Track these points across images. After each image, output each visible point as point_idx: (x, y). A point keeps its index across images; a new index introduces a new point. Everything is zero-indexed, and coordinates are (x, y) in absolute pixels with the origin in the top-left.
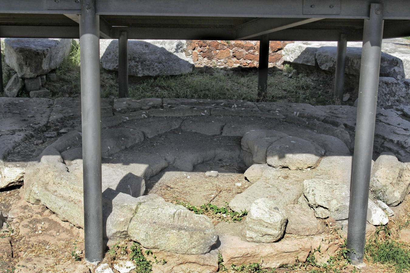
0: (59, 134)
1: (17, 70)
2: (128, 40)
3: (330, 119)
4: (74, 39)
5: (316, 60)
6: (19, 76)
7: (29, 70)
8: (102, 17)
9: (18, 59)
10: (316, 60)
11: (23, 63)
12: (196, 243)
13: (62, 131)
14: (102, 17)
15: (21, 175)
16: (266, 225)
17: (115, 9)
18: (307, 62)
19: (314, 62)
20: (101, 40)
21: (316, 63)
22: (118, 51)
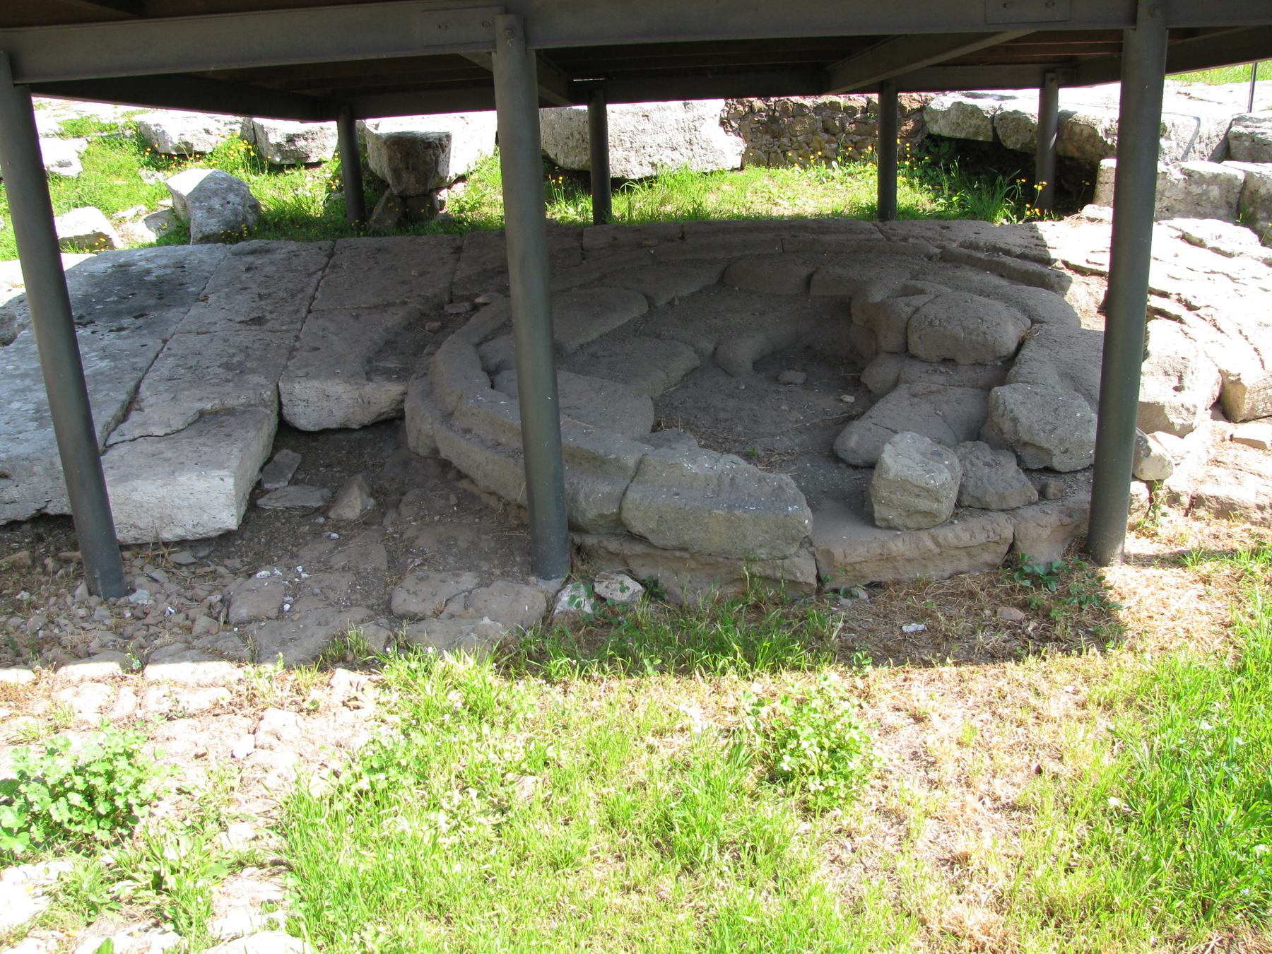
0: (476, 308)
1: (390, 182)
2: (370, 123)
3: (1033, 252)
4: (258, 121)
5: (994, 129)
6: (395, 192)
7: (413, 180)
8: (538, 52)
9: (390, 159)
10: (994, 129)
11: (401, 166)
12: (767, 536)
13: (480, 300)
14: (538, 52)
15: (399, 398)
16: (916, 490)
17: (574, 28)
18: (977, 134)
19: (990, 133)
20: (541, 110)
21: (995, 135)
22: (587, 129)
